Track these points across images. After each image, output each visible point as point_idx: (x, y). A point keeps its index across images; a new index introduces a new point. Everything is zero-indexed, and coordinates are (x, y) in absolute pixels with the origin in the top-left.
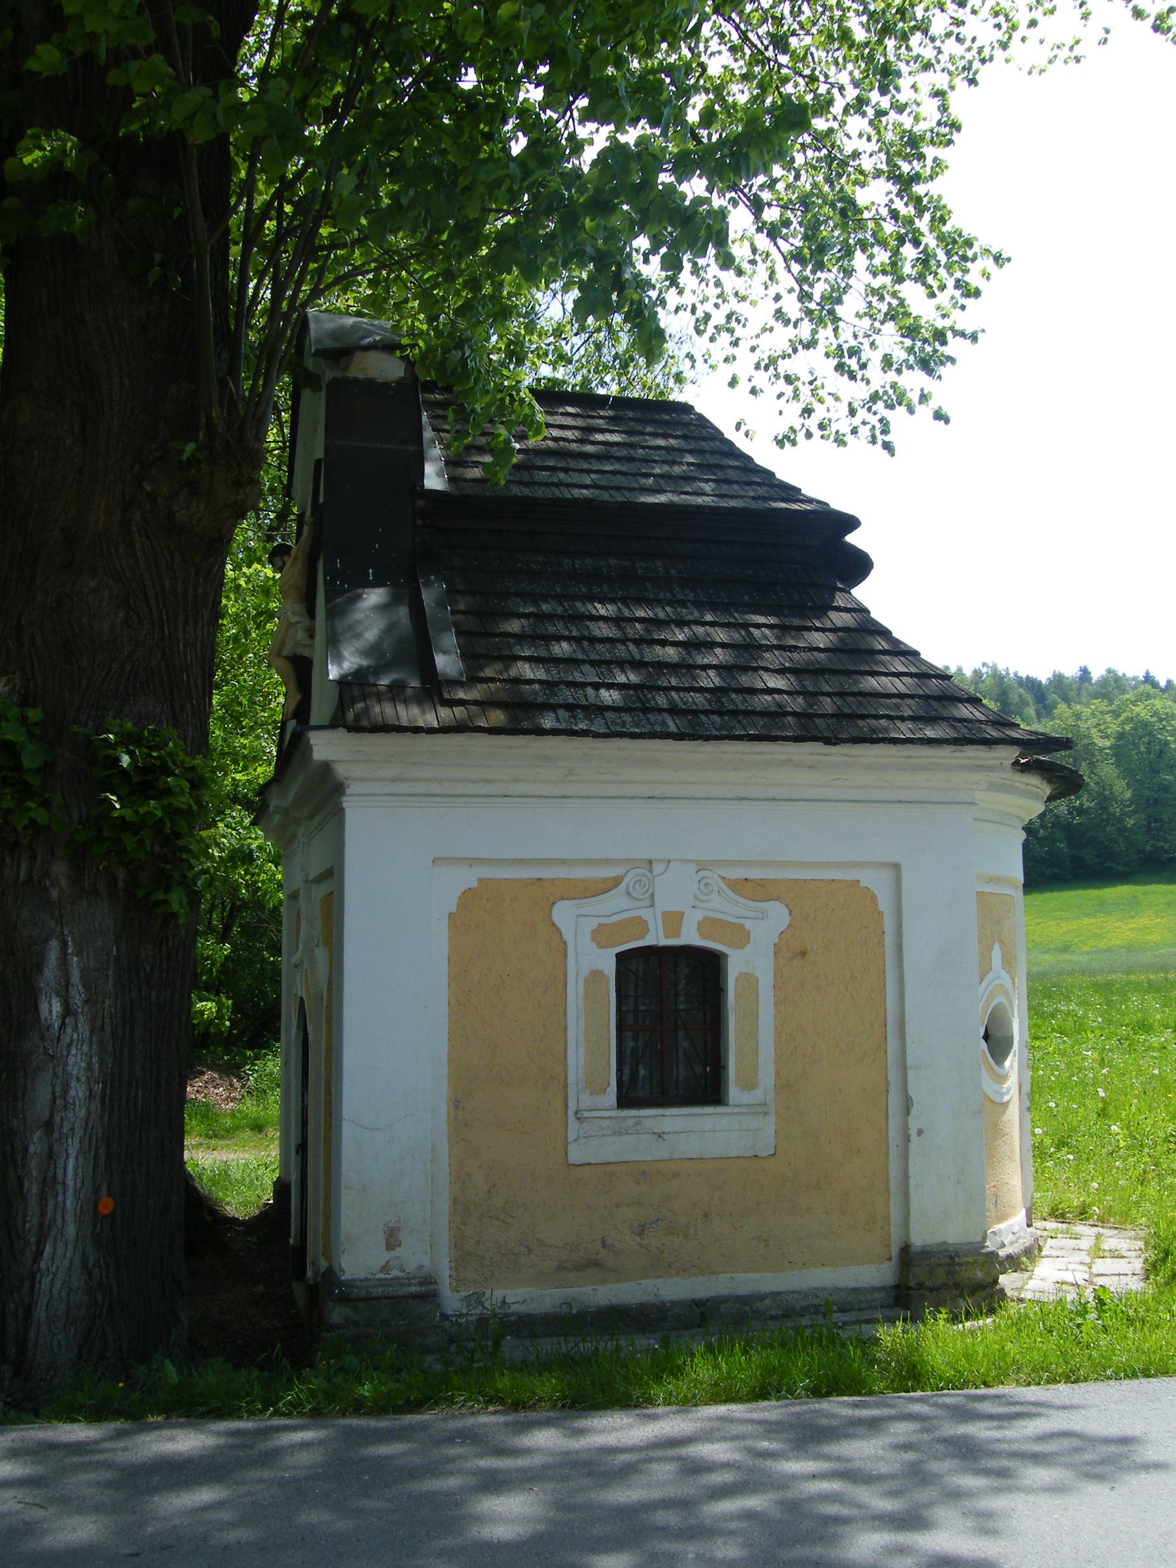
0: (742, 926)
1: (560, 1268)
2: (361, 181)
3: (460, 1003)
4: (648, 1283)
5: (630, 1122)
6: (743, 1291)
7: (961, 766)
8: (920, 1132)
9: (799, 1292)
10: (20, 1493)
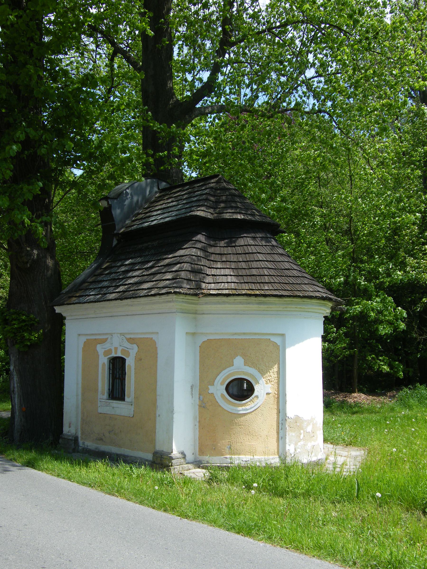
0: (128, 351)
1: (96, 439)
2: (396, 252)
3: (84, 370)
4: (110, 447)
5: (108, 403)
6: (126, 454)
7: (183, 301)
8: (159, 416)
9: (135, 457)
10: (9, 469)
